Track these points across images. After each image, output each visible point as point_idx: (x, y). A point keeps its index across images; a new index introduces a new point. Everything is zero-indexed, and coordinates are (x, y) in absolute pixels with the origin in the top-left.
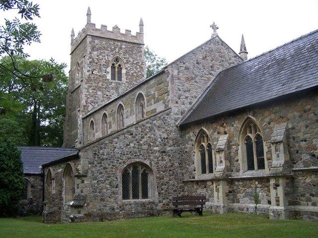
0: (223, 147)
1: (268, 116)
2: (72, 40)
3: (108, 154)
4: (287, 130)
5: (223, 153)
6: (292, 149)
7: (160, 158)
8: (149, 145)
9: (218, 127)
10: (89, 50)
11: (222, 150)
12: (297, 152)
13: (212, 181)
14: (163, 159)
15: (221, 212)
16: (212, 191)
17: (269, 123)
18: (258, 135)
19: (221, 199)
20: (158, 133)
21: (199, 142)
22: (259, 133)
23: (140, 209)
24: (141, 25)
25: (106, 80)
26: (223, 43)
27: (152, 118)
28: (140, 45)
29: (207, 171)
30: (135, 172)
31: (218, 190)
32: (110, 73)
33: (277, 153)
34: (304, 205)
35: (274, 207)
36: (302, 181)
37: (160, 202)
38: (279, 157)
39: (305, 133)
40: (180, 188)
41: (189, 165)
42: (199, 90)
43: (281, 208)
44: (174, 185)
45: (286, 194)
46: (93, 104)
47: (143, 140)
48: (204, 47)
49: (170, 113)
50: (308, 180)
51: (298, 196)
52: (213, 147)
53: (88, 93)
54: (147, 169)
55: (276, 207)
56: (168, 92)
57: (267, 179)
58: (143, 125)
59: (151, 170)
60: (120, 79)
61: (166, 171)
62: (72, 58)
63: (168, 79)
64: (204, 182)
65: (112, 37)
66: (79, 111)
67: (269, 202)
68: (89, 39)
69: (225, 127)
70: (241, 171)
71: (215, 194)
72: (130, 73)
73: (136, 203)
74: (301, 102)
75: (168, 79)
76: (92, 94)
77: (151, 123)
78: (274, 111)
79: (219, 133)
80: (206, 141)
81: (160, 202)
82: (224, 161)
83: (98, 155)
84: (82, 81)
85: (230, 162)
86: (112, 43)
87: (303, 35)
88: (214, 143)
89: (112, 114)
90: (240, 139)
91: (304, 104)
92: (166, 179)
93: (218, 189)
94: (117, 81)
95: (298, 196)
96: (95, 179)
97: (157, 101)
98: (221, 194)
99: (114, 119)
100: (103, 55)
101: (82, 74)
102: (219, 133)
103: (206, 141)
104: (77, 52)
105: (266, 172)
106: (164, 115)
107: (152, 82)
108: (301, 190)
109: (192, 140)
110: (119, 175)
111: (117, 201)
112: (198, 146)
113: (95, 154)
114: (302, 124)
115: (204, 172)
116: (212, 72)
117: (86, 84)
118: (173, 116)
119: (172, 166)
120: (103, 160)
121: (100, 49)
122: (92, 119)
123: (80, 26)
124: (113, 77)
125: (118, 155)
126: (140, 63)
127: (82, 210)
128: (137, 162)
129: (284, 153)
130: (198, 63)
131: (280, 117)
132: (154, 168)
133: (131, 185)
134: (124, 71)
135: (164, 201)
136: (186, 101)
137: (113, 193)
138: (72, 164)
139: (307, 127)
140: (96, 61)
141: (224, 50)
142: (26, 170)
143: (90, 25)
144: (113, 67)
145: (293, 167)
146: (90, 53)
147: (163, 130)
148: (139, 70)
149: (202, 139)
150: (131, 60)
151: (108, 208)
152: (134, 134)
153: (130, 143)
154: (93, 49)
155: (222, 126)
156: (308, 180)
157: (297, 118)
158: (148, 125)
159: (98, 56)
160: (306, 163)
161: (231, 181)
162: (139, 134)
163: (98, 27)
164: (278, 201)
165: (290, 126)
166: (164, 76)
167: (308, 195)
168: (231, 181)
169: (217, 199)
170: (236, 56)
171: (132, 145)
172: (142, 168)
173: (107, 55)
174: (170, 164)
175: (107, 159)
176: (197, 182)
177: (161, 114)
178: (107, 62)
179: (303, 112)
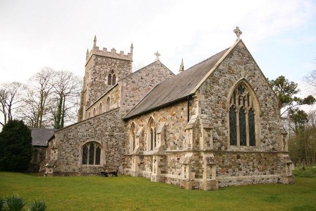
3: (73, 136)
4: (165, 126)
14: (111, 140)
15: (187, 188)
23: (93, 171)
24: (132, 48)
26: (162, 65)
30: (92, 148)
42: (141, 96)
48: (147, 68)
49: (119, 111)
70: (147, 151)
73: (90, 167)
96: (64, 151)
110: (80, 149)
111: (77, 164)
116: (153, 85)
118: (120, 113)
120: (70, 139)
121: (101, 64)
124: (109, 83)
125: (80, 137)
130: (142, 79)
136: (131, 103)
137: (75, 160)
140: (98, 72)
141: (162, 70)
142: (35, 143)
143: (96, 48)
150: (123, 72)
154: (96, 64)
158: (102, 118)
159: (99, 69)
163: (101, 49)
168: (142, 157)
171: (90, 130)
174: (115, 144)
175: (72, 139)
178: (105, 73)
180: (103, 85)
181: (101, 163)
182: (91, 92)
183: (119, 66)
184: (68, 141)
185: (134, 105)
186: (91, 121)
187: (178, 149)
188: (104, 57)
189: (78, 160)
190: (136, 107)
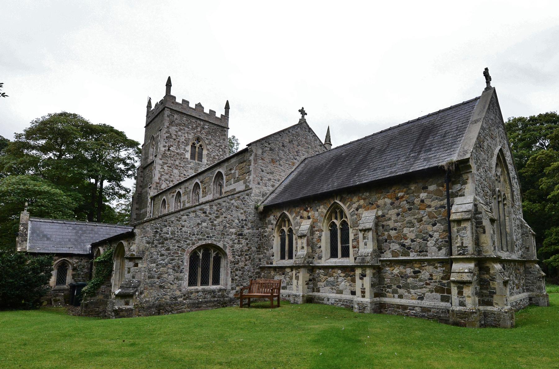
0: (305, 232)
1: (357, 202)
2: (148, 112)
3: (173, 233)
4: (377, 217)
5: (306, 238)
6: (381, 238)
7: (236, 241)
8: (225, 226)
9: (301, 211)
10: (167, 124)
11: (304, 236)
12: (386, 241)
13: (292, 268)
14: (239, 243)
16: (291, 278)
17: (357, 210)
18: (344, 221)
19: (301, 288)
20: (235, 214)
21: (280, 226)
22: (346, 220)
24: (227, 107)
25: (184, 158)
27: (230, 197)
28: (225, 128)
29: (287, 257)
30: (206, 256)
31: (297, 278)
32: (190, 151)
33: (365, 241)
34: (390, 297)
35: (358, 298)
36: (389, 272)
37: (232, 289)
38: (366, 245)
39: (396, 221)
40: (256, 274)
41: (267, 250)
42: (283, 174)
43: (367, 300)
44: (249, 271)
45: (373, 286)
46: (168, 182)
47: (218, 220)
48: (291, 131)
50: (396, 271)
51: (384, 287)
52: (294, 232)
53: (162, 170)
54: (220, 252)
55: (361, 299)
56: (249, 172)
57: (352, 269)
58: (219, 204)
59: (225, 254)
60: (200, 159)
61: (242, 255)
62: (146, 132)
63: (252, 158)
64: (281, 269)
65: (194, 114)
66: (150, 188)
67: (353, 293)
68: (167, 112)
69: (308, 212)
70: (323, 259)
71: (294, 281)
72: (212, 155)
73: (204, 291)
74: (393, 189)
75: (252, 158)
76: (166, 171)
77: (228, 203)
78: (363, 196)
79: (301, 217)
80: (287, 225)
81: (232, 289)
82: (306, 248)
83: (160, 234)
84: (156, 156)
85: (312, 248)
86: (194, 121)
87: (401, 123)
88: (296, 228)
89: (186, 193)
90: (325, 224)
91: (397, 191)
92: (241, 264)
93: (298, 277)
94: (196, 161)
95: (384, 287)
96: (154, 261)
97: (238, 180)
98: (300, 282)
99: (188, 198)
100: (183, 131)
101: (157, 149)
102: (301, 217)
103: (287, 225)
104: (153, 124)
105: (349, 261)
106: (244, 196)
107: (233, 161)
108: (387, 281)
109: (272, 224)
110: (186, 258)
112: (278, 230)
113: (156, 232)
114: (393, 212)
115: (283, 257)
116: (298, 158)
117: (161, 159)
119: (249, 250)
120: (166, 239)
122: (165, 197)
123: (158, 96)
124: (193, 156)
126: (223, 146)
127: (131, 301)
128: (209, 245)
129: (373, 241)
131: (370, 203)
132: (228, 251)
133: (200, 270)
134: (205, 152)
135: (238, 288)
138: (125, 243)
139: (398, 214)
140: (174, 137)
143: (169, 97)
144: (193, 146)
145: (380, 257)
146: (168, 127)
147: (242, 211)
148: (221, 153)
149: (283, 224)
151: (168, 297)
152: (208, 212)
153: (202, 222)
155: (306, 210)
156: (396, 271)
157: (389, 205)
158: (224, 204)
159: (176, 132)
160: (394, 253)
161: (312, 269)
162: (214, 213)
164: (363, 292)
165: (380, 213)
166: (247, 155)
167: (394, 287)
168: (312, 269)
169: (297, 287)
170: (321, 145)
172: (214, 252)
173: (187, 133)
175: (171, 239)
176: (275, 268)
177: (241, 194)
178: (187, 140)
179: (395, 199)
180: (183, 159)
181: (67, 281)
182: (162, 168)
183: (208, 133)
184: (163, 243)
185: (273, 186)
186: (207, 207)
187: (413, 256)
188: (185, 114)
189: (181, 279)
190: (276, 189)
